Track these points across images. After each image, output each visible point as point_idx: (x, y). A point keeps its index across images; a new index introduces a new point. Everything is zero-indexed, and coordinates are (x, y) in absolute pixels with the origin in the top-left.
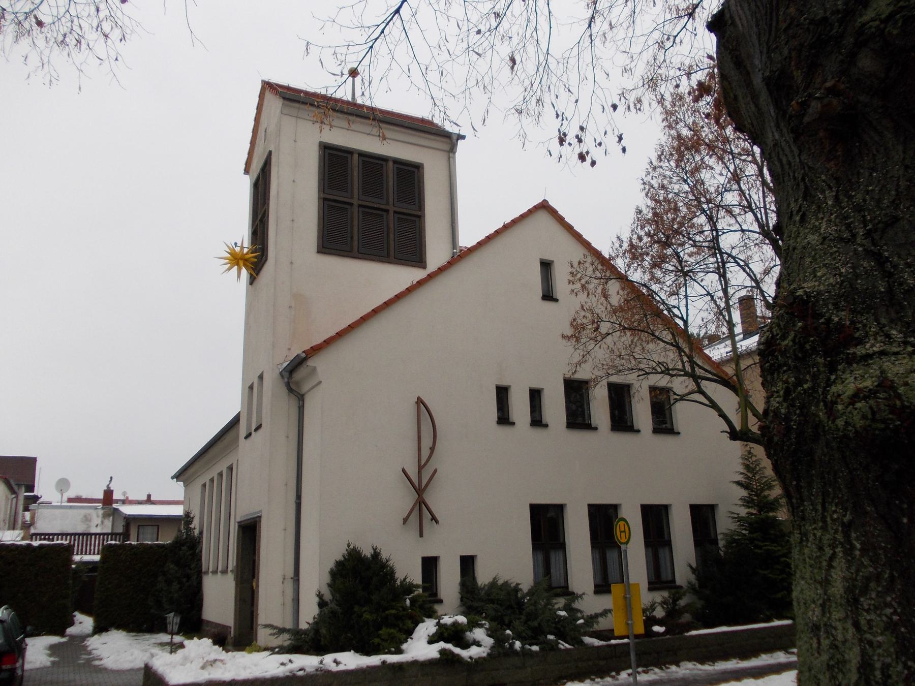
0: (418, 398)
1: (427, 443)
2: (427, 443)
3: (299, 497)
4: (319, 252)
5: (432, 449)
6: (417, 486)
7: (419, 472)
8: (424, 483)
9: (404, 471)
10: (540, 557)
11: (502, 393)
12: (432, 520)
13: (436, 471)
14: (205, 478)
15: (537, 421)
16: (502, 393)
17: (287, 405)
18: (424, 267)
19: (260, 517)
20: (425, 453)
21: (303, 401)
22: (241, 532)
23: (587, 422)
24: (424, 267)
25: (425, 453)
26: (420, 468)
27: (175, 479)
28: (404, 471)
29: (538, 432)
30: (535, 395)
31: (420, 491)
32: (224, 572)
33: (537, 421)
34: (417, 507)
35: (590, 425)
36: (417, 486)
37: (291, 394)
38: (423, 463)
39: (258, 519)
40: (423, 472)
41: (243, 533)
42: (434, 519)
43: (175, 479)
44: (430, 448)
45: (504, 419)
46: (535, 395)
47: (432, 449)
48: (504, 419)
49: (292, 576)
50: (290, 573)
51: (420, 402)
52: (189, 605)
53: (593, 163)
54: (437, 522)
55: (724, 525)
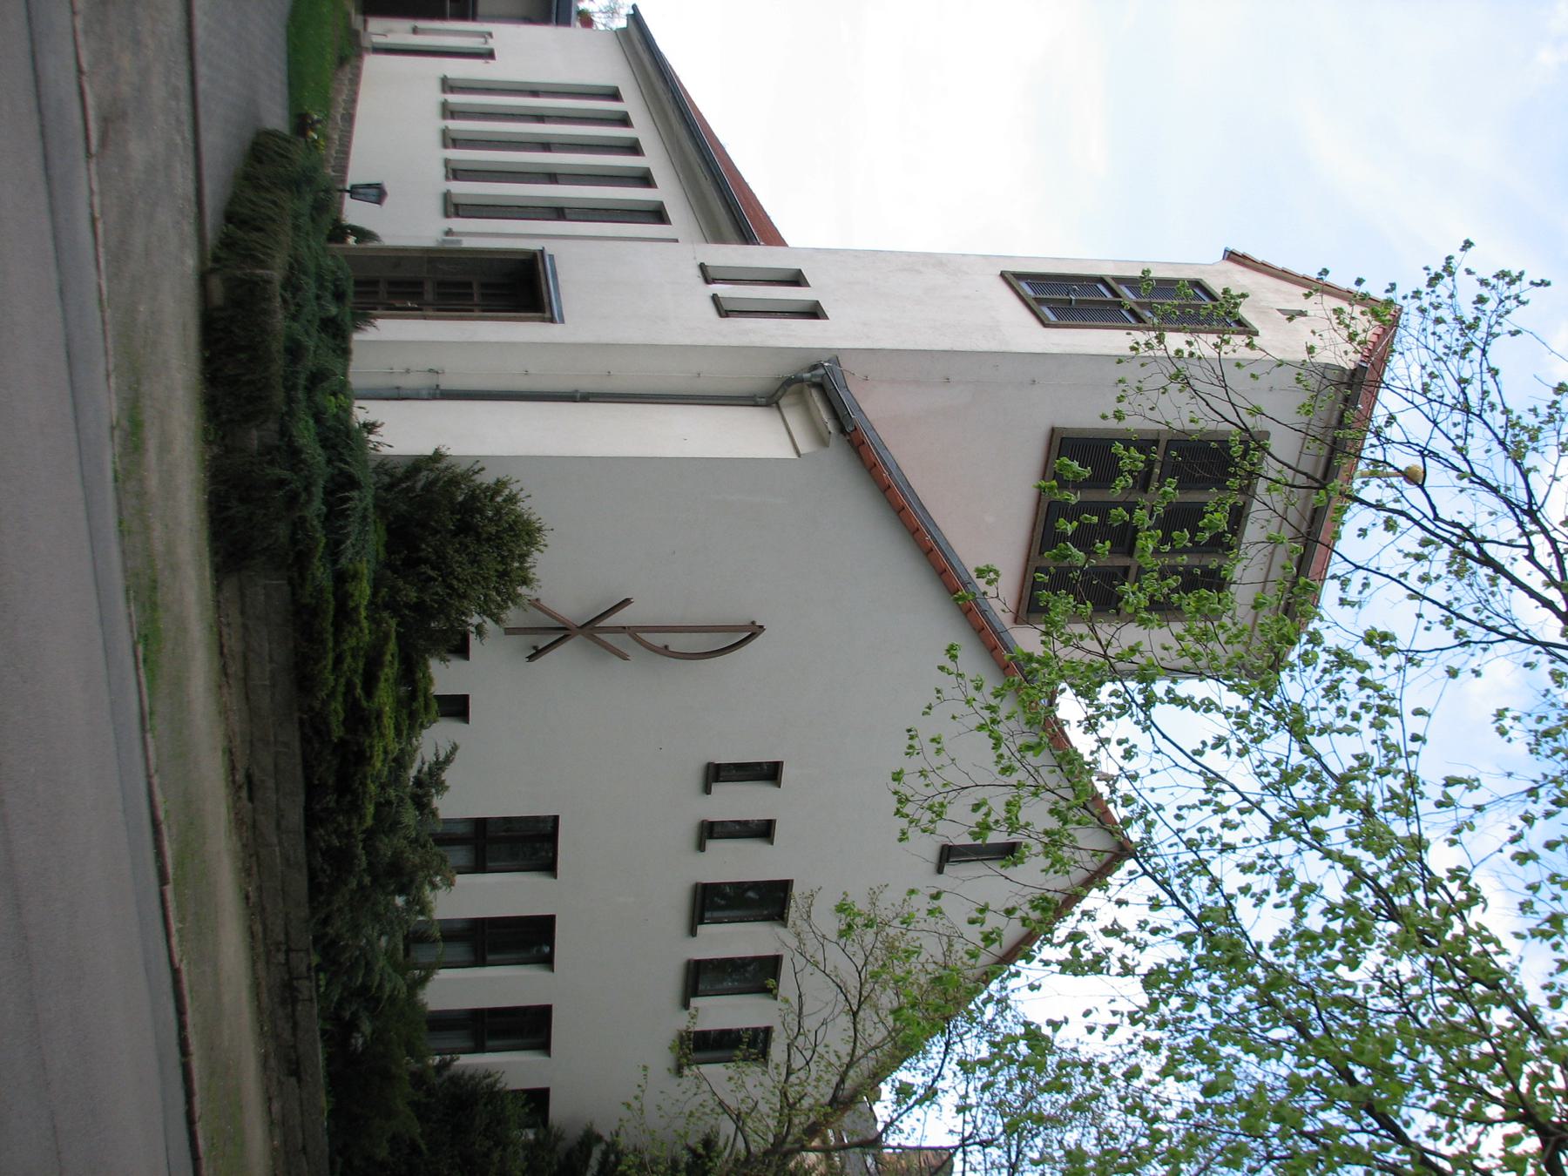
0: (761, 627)
1: (678, 642)
2: (678, 642)
3: (586, 398)
4: (1053, 430)
5: (665, 651)
6: (601, 624)
7: (623, 629)
8: (602, 636)
9: (626, 602)
10: (461, 830)
11: (770, 773)
12: (535, 648)
13: (624, 657)
14: (631, 104)
15: (709, 831)
16: (770, 773)
17: (759, 376)
18: (1016, 621)
19: (552, 320)
20: (657, 640)
21: (767, 405)
22: (523, 257)
23: (707, 915)
24: (1016, 621)
25: (657, 640)
26: (633, 631)
27: (632, 12)
28: (626, 602)
29: (689, 833)
30: (764, 831)
31: (591, 629)
32: (454, 208)
33: (709, 831)
34: (557, 624)
35: (702, 922)
36: (601, 624)
37: (780, 383)
38: (644, 636)
39: (547, 315)
40: (625, 636)
41: (523, 262)
42: (537, 653)
43: (632, 12)
44: (666, 647)
45: (716, 774)
46: (764, 831)
47: (665, 651)
48: (716, 774)
49: (442, 387)
50: (447, 383)
51: (754, 631)
52: (533, 1105)
53: (1510, 740)
54: (531, 658)
55: (427, 888)
